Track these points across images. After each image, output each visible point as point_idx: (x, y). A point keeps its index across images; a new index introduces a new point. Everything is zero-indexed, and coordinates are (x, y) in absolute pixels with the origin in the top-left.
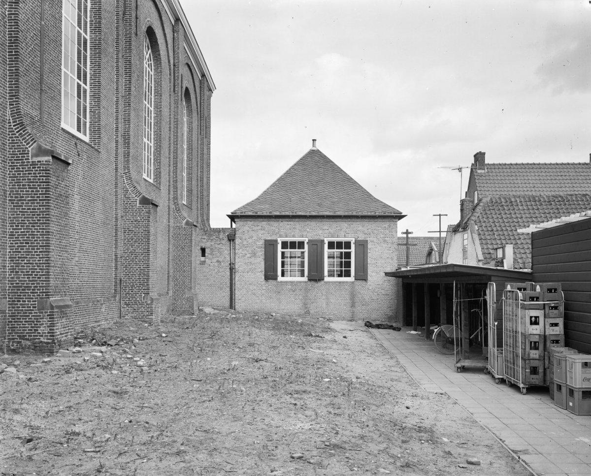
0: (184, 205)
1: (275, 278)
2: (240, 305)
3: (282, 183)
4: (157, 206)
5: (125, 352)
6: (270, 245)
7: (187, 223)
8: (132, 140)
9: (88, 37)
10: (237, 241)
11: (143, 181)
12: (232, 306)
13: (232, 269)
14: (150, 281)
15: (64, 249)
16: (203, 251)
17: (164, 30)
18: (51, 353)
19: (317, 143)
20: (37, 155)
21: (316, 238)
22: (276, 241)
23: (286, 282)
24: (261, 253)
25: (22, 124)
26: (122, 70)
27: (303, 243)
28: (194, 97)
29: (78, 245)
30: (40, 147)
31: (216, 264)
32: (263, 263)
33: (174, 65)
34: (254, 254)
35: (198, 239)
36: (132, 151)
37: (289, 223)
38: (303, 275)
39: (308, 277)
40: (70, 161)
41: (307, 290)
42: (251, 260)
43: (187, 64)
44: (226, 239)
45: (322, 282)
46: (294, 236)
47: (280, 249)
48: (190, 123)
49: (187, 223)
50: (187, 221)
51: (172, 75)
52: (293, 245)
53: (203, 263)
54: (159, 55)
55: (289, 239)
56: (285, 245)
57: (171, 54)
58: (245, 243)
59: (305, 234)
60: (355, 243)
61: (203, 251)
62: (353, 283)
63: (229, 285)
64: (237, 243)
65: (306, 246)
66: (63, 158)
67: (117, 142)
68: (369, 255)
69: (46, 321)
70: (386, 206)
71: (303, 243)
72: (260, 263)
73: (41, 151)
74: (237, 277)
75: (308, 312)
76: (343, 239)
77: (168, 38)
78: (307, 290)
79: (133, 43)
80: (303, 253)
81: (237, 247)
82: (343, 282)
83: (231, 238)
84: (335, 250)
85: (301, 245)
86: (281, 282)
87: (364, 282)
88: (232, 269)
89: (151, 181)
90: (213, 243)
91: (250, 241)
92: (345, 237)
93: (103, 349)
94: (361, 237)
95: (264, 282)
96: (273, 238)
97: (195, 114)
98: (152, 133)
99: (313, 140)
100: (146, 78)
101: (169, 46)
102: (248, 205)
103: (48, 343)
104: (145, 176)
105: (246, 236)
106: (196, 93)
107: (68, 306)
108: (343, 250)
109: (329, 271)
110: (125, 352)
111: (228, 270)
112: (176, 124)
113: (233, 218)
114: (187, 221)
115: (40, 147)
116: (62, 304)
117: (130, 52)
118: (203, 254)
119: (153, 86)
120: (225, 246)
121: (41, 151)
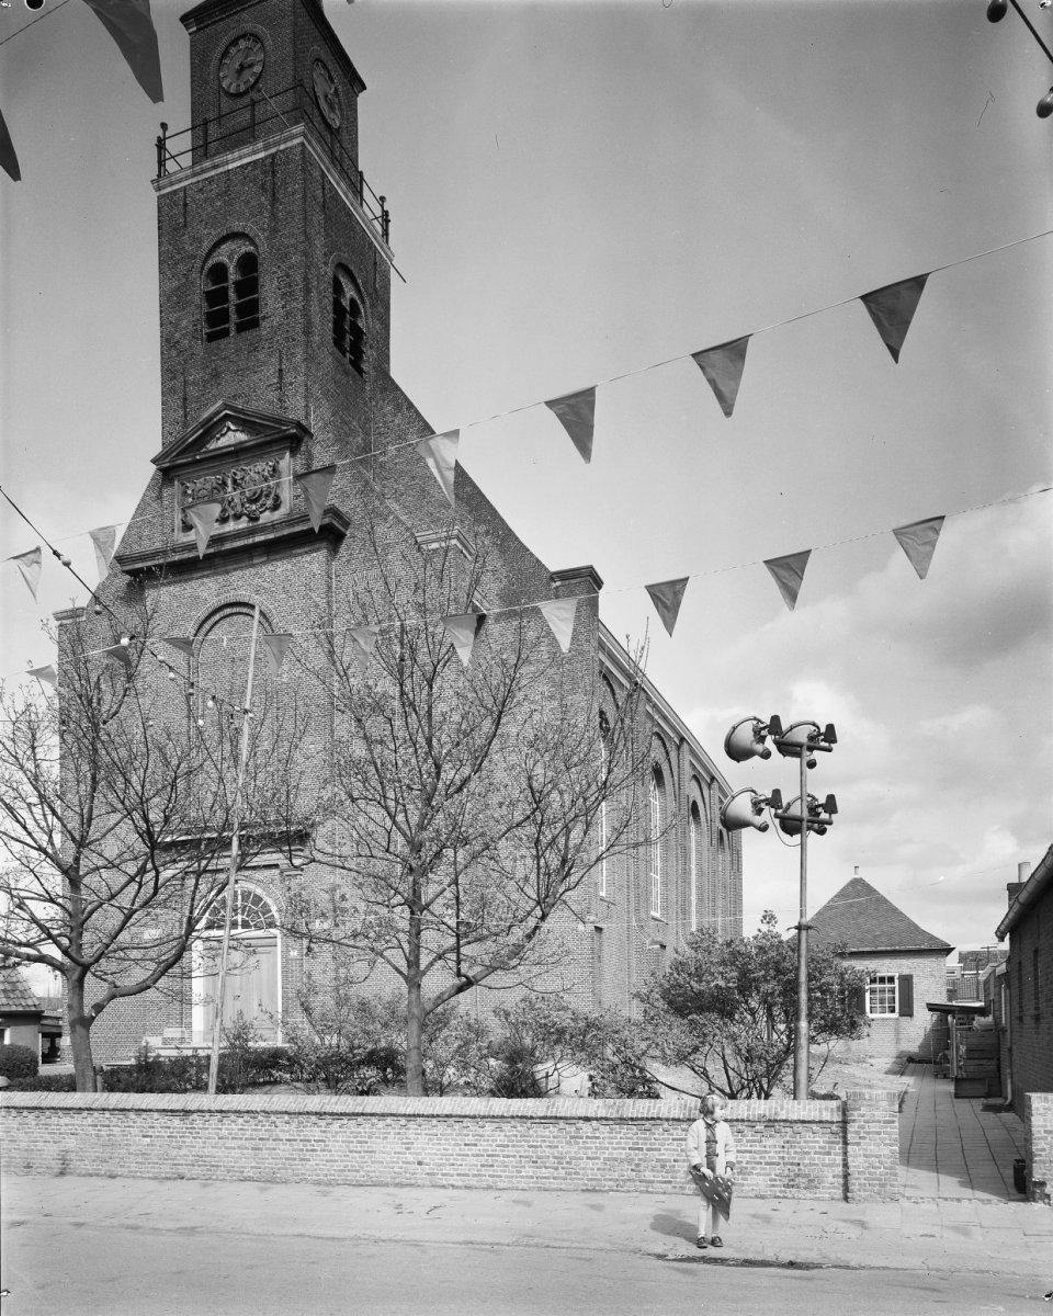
38: (893, 1011)
70: (933, 938)
73: (656, 943)
85: (891, 980)
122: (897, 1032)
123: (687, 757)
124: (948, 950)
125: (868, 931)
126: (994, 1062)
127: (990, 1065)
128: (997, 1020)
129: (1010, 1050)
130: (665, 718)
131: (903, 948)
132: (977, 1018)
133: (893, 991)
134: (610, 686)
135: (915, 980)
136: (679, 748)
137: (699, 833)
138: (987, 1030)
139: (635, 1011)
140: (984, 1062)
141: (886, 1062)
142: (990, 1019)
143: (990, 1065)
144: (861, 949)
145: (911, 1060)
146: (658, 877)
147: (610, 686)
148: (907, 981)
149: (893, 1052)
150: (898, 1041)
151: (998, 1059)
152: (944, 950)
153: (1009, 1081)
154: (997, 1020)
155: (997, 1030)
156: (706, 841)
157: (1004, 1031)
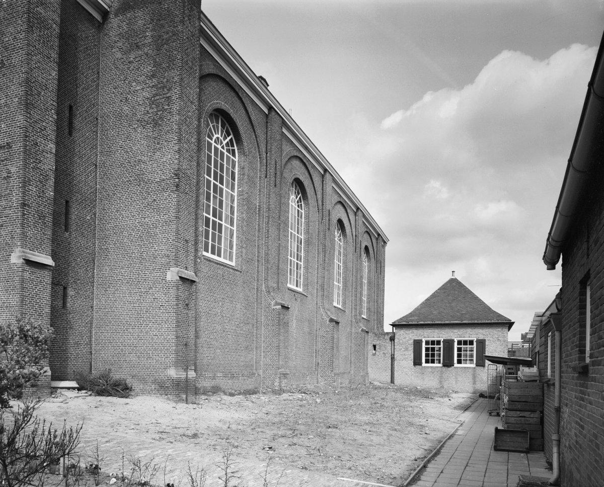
0: (363, 318)
1: (420, 364)
2: (397, 381)
3: (428, 303)
4: (339, 323)
5: (313, 396)
6: (417, 344)
7: (362, 330)
8: (326, 287)
9: (302, 237)
10: (396, 341)
11: (334, 308)
12: (392, 381)
13: (393, 359)
14: (334, 364)
15: (286, 347)
16: (375, 347)
17: (348, 217)
18: (280, 394)
19: (455, 273)
20: (275, 306)
21: (449, 338)
22: (421, 340)
23: (428, 367)
24: (411, 348)
25: (269, 292)
26: (321, 250)
27: (440, 341)
28: (372, 249)
29: (295, 345)
30: (276, 302)
31: (382, 355)
32: (412, 354)
33: (356, 236)
34: (407, 349)
35: (371, 339)
36: (325, 293)
37: (407, 332)
38: (440, 363)
39: (443, 364)
40: (290, 307)
41: (442, 372)
42: (404, 353)
43: (367, 232)
44: (389, 340)
45: (453, 367)
46: (433, 338)
47: (456, 346)
48: (369, 267)
49: (362, 330)
50: (362, 329)
51: (354, 242)
52: (465, 343)
53: (374, 355)
54: (346, 233)
55: (430, 339)
56: (459, 343)
57: (354, 230)
58: (401, 341)
59: (441, 335)
60: (476, 342)
61: (375, 347)
62: (475, 368)
63: (390, 368)
64: (395, 341)
65: (442, 343)
66: (286, 306)
67: (317, 289)
68: (487, 349)
69: (277, 380)
70: (500, 316)
71: (440, 341)
72: (410, 355)
73: (277, 304)
74: (396, 363)
75: (442, 387)
76: (436, 339)
77: (351, 222)
78: (442, 372)
79: (327, 235)
80: (440, 348)
81: (396, 344)
82: (468, 368)
83: (392, 339)
84: (468, 346)
85: (471, 343)
86: (425, 367)
87: (482, 368)
88: (393, 359)
89: (340, 306)
90: (380, 342)
91: (404, 340)
92: (469, 337)
93: (303, 395)
94: (481, 337)
95: (413, 367)
96: (420, 338)
97: (373, 260)
98: (341, 278)
99: (453, 272)
100: (337, 247)
101: (352, 225)
102: (403, 317)
103: (278, 390)
104: (335, 304)
105: (402, 337)
106: (374, 250)
107: (287, 374)
108: (430, 346)
109: (426, 360)
110: (313, 396)
111: (390, 359)
112: (359, 270)
113: (393, 325)
114: (362, 329)
115: (276, 302)
116: (285, 373)
117: (325, 238)
118: (375, 349)
119: (342, 251)
120: (388, 344)
121: (277, 304)
122: (474, 377)
123: (330, 185)
124: (509, 325)
125: (458, 311)
126: (537, 415)
127: (534, 417)
128: (542, 372)
129: (558, 410)
130: (306, 148)
131: (480, 322)
132: (521, 368)
133: (472, 351)
134: (240, 99)
135: (487, 343)
136: (323, 176)
137: (346, 242)
138: (531, 381)
139: (535, 366)
140: (527, 414)
141: (461, 398)
142: (534, 370)
143: (534, 417)
144: (452, 322)
145: (482, 395)
146: (302, 263)
147: (240, 99)
148: (481, 344)
149: (471, 390)
150: (474, 383)
151: (542, 412)
152: (506, 323)
153: (555, 450)
154: (542, 372)
155: (542, 382)
156: (351, 249)
157: (550, 384)
